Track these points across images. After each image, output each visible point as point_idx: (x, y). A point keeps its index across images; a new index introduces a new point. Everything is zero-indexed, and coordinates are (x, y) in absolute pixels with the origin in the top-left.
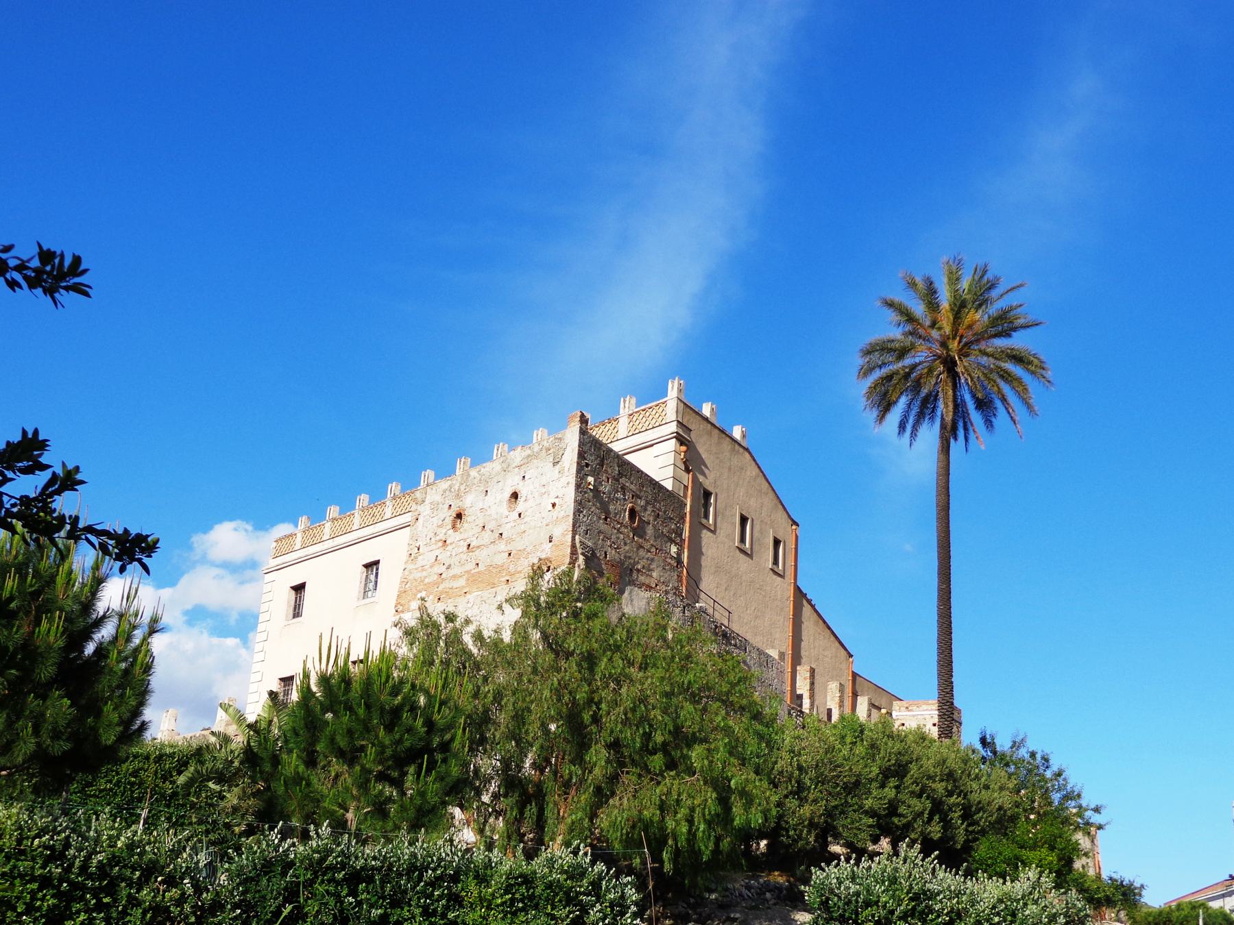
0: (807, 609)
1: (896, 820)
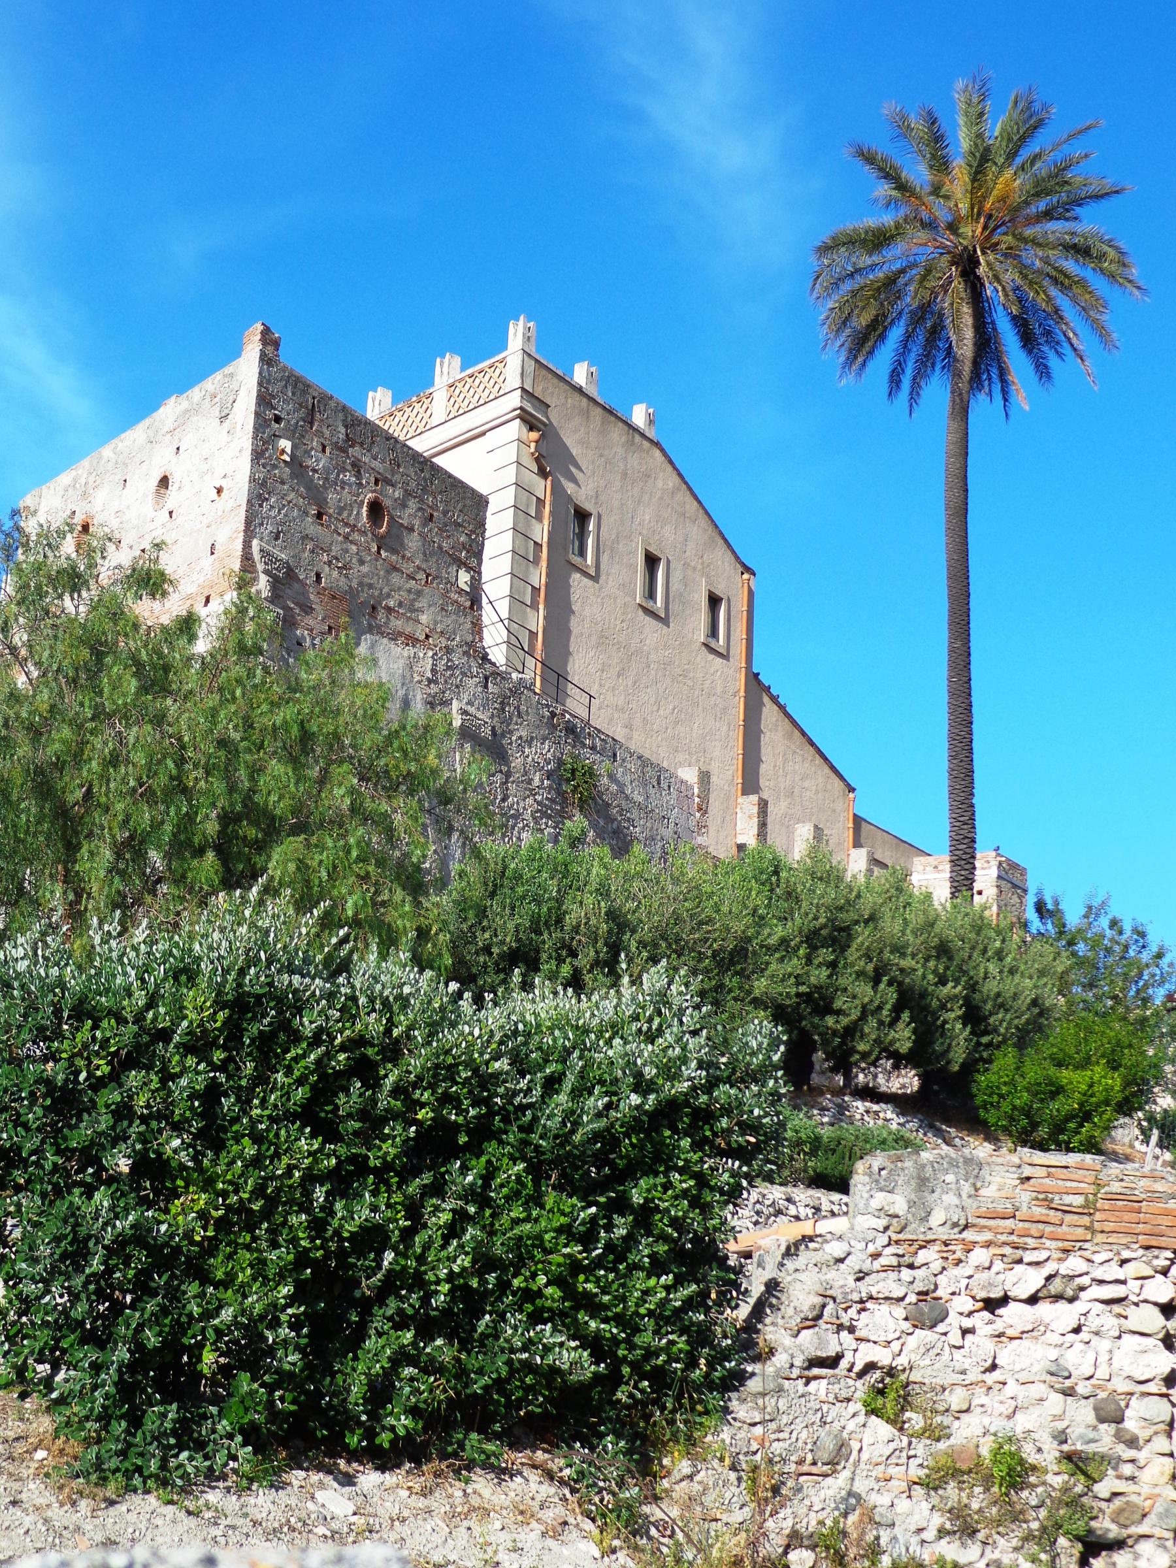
0: (769, 712)
1: (830, 1021)
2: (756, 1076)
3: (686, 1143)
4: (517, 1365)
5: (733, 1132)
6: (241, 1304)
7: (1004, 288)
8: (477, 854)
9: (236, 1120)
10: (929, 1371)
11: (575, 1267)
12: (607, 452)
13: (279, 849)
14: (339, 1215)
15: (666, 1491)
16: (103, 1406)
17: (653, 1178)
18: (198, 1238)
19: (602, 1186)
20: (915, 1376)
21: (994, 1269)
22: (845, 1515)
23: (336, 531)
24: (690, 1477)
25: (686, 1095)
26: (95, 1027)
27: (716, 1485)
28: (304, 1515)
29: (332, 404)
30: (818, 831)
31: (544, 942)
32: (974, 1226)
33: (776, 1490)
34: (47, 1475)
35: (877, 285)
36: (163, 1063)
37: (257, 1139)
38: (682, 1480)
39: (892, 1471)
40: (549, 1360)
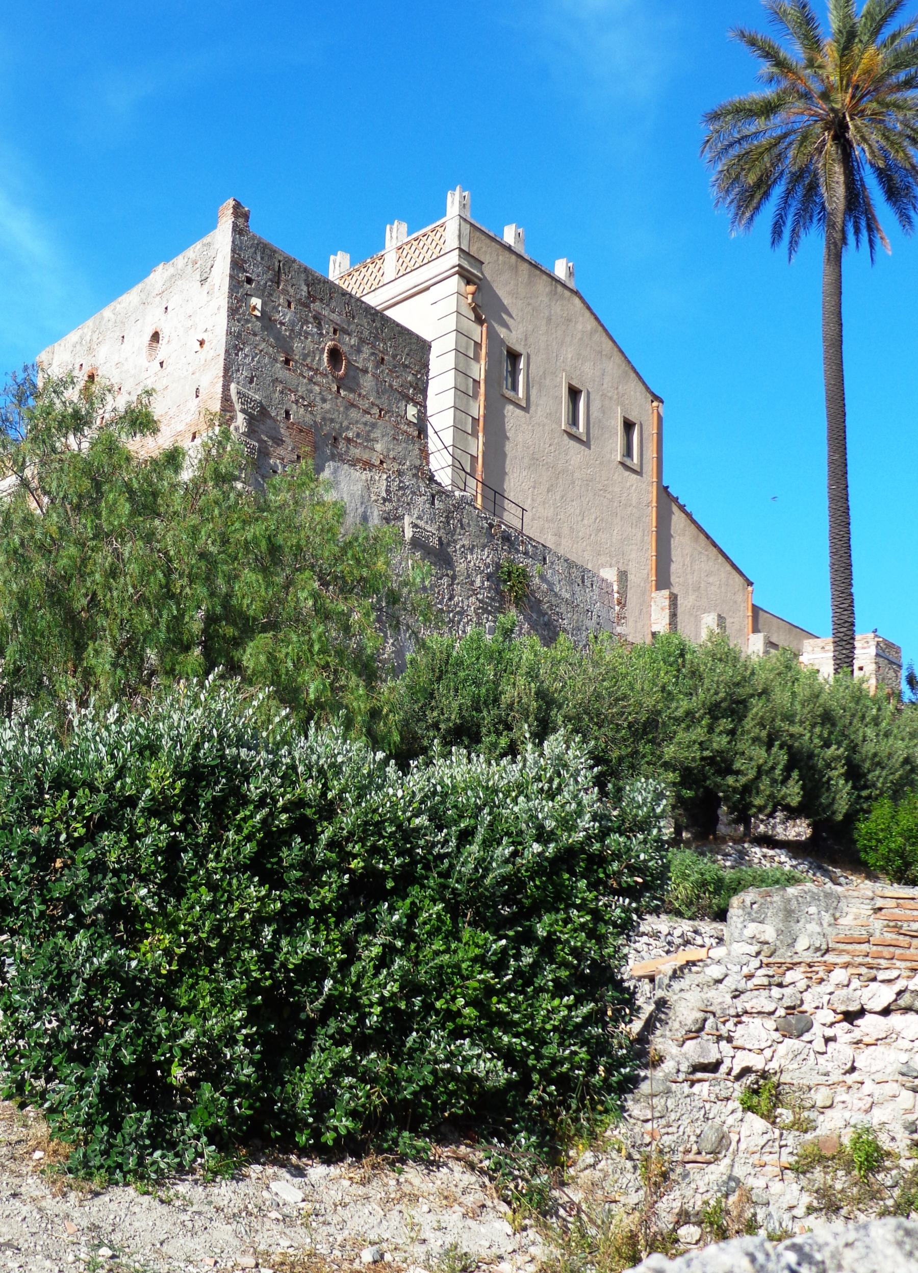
0: (678, 520)
1: (730, 780)
2: (643, 826)
3: (582, 884)
4: (440, 1074)
5: (623, 874)
6: (203, 1026)
7: (870, 146)
8: (422, 645)
9: (194, 872)
10: (797, 1073)
11: (489, 990)
12: (532, 301)
13: (251, 644)
14: (285, 950)
15: (572, 1178)
16: (87, 1114)
17: (556, 916)
18: (164, 972)
19: (510, 921)
20: (785, 1078)
21: (852, 986)
22: (727, 1196)
23: (301, 375)
24: (593, 1166)
25: (582, 843)
26: (72, 795)
27: (614, 1172)
28: (260, 1202)
29: (296, 266)
30: (721, 619)
31: (484, 719)
32: (834, 950)
33: (665, 1176)
34: (43, 1172)
35: (760, 150)
36: (131, 825)
37: (213, 887)
38: (586, 1169)
39: (766, 1158)
40: (468, 1069)
